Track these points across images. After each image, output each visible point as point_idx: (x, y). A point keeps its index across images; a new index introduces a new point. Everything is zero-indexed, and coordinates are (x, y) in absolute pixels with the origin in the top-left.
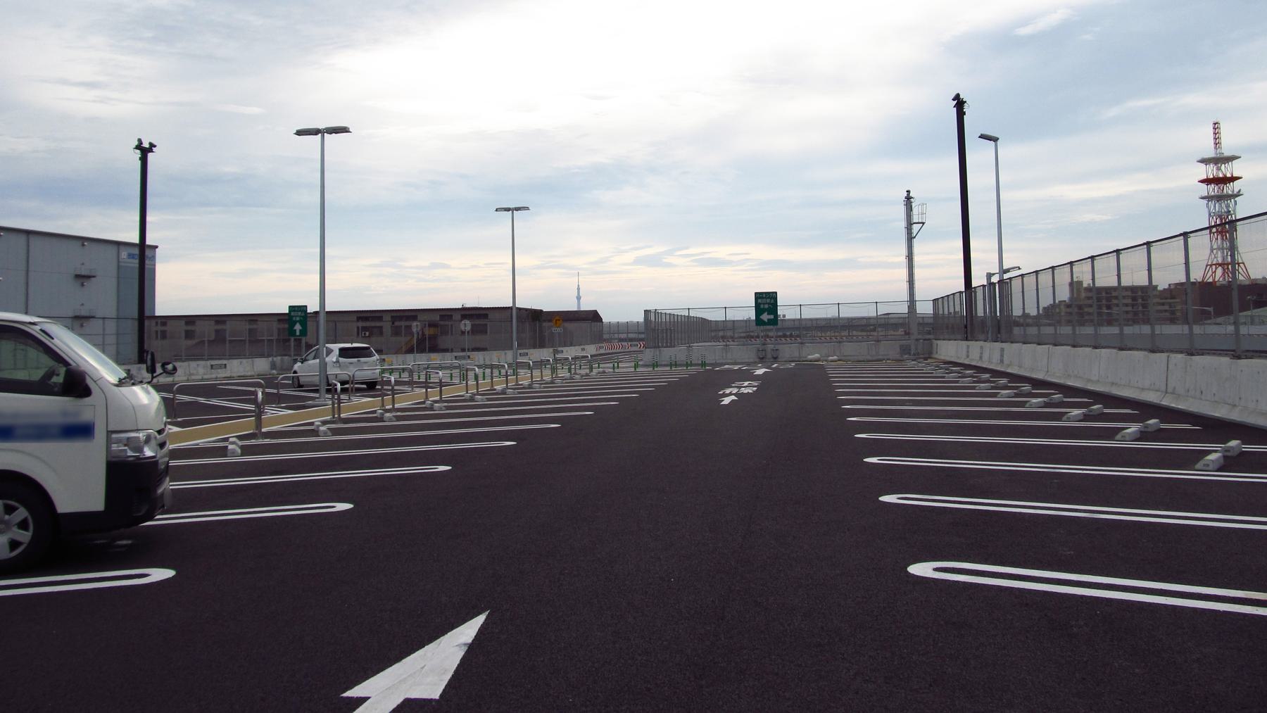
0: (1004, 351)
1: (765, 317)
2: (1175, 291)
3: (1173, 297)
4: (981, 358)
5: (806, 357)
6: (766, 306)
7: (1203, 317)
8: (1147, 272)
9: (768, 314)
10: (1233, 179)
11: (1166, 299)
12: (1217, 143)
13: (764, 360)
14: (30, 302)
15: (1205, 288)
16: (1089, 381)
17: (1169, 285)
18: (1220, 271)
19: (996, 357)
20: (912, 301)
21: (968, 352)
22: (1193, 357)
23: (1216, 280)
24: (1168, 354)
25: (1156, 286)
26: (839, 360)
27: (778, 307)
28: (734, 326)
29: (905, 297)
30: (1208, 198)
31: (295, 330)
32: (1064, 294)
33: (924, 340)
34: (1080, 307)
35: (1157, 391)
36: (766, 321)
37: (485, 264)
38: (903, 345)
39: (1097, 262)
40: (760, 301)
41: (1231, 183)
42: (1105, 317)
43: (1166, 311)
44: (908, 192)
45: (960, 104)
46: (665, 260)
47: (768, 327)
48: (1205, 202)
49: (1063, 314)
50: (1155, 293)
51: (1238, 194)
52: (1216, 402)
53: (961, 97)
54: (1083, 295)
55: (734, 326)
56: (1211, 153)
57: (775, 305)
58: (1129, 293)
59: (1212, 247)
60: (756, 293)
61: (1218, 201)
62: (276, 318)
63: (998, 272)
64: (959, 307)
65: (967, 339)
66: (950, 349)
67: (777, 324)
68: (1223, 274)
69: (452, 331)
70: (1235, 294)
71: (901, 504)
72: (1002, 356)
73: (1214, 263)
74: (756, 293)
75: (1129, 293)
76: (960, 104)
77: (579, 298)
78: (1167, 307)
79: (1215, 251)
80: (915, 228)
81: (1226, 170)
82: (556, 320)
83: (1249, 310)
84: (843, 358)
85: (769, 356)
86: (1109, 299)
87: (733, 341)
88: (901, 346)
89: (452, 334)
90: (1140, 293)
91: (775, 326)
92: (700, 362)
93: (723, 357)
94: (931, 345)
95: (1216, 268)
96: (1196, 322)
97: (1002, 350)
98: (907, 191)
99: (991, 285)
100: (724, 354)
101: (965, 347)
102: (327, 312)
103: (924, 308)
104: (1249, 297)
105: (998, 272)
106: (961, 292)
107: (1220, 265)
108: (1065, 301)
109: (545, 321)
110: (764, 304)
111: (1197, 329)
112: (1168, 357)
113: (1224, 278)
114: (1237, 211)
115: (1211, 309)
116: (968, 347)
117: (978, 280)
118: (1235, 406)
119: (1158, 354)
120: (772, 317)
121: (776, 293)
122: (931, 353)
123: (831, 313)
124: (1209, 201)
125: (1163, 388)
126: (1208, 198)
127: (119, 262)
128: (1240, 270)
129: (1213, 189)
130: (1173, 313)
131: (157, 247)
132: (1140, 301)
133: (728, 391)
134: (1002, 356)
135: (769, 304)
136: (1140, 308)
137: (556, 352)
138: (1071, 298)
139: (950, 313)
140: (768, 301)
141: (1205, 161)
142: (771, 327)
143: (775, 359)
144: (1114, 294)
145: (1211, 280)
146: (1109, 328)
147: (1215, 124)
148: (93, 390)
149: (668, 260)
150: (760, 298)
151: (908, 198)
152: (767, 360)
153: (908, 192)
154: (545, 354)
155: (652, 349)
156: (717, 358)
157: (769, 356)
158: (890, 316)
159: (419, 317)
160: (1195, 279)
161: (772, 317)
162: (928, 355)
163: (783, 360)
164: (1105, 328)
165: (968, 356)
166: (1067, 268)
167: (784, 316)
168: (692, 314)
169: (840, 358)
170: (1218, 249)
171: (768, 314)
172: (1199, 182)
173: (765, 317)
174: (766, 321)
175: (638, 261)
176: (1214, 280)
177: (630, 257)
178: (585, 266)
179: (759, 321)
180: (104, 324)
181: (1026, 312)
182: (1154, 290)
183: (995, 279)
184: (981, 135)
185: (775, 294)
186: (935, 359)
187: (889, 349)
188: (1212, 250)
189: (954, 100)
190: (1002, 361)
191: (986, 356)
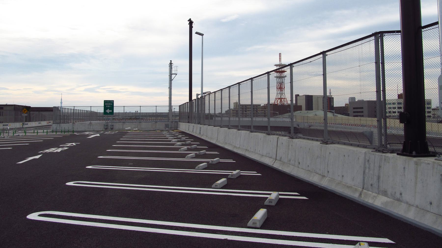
0: (201, 128)
1: (108, 111)
2: (265, 107)
3: (265, 109)
5: (125, 128)
6: (109, 106)
7: (274, 115)
9: (109, 110)
11: (263, 109)
12: (280, 60)
13: (107, 130)
15: (275, 106)
16: (235, 147)
17: (264, 105)
18: (279, 101)
19: (198, 131)
20: (170, 106)
21: (189, 128)
22: (294, 140)
23: (278, 103)
24: (278, 136)
26: (138, 130)
27: (114, 107)
28: (119, 115)
29: (167, 104)
31: (109, 112)
33: (175, 122)
35: (270, 158)
36: (109, 113)
37: (24, 89)
38: (166, 124)
40: (106, 104)
42: (244, 114)
44: (171, 61)
45: (191, 22)
46: (96, 90)
48: (276, 78)
50: (260, 107)
52: (309, 171)
53: (191, 20)
55: (119, 115)
56: (278, 63)
59: (277, 93)
60: (104, 101)
61: (280, 78)
62: (13, 107)
63: (201, 93)
65: (189, 122)
66: (184, 127)
68: (280, 102)
69: (3, 114)
70: (209, 116)
72: (200, 131)
74: (104, 101)
76: (191, 22)
77: (61, 103)
78: (263, 112)
80: (173, 76)
82: (24, 111)
83: (288, 113)
84: (140, 129)
85: (109, 128)
86: (246, 109)
87: (103, 121)
88: (165, 124)
89: (3, 115)
90: (255, 107)
91: (112, 115)
92: (61, 130)
93: (89, 128)
94: (178, 124)
95: (278, 100)
96: (271, 117)
97: (200, 128)
98: (171, 61)
99: (198, 98)
100: (89, 127)
101: (188, 126)
105: (201, 93)
106: (188, 103)
107: (279, 99)
108: (232, 109)
109: (31, 111)
110: (108, 105)
111: (272, 119)
112: (278, 138)
114: (285, 82)
115: (278, 113)
117: (194, 97)
118: (324, 176)
119: (272, 136)
120: (111, 111)
121: (113, 101)
122: (177, 127)
123: (153, 110)
125: (274, 156)
126: (277, 77)
130: (265, 113)
132: (255, 109)
134: (200, 131)
135: (110, 105)
137: (23, 124)
138: (234, 108)
140: (110, 104)
142: (111, 115)
143: (112, 129)
144: (247, 107)
145: (276, 103)
146: (246, 118)
147: (280, 54)
149: (98, 90)
150: (106, 103)
151: (171, 64)
152: (108, 130)
153: (171, 61)
154: (18, 125)
155: (56, 124)
156: (86, 128)
157: (109, 128)
158: (175, 112)
159: (4, 108)
160: (272, 103)
161: (111, 111)
162: (176, 128)
163: (115, 130)
164: (244, 118)
165: (189, 130)
166: (227, 90)
169: (139, 129)
170: (279, 93)
171: (109, 110)
173: (108, 111)
174: (109, 113)
175: (86, 90)
176: (277, 103)
177: (83, 88)
178: (65, 91)
179: (105, 113)
183: (199, 97)
184: (196, 32)
186: (178, 130)
187: (160, 125)
188: (277, 94)
189: (188, 21)
190: (200, 133)
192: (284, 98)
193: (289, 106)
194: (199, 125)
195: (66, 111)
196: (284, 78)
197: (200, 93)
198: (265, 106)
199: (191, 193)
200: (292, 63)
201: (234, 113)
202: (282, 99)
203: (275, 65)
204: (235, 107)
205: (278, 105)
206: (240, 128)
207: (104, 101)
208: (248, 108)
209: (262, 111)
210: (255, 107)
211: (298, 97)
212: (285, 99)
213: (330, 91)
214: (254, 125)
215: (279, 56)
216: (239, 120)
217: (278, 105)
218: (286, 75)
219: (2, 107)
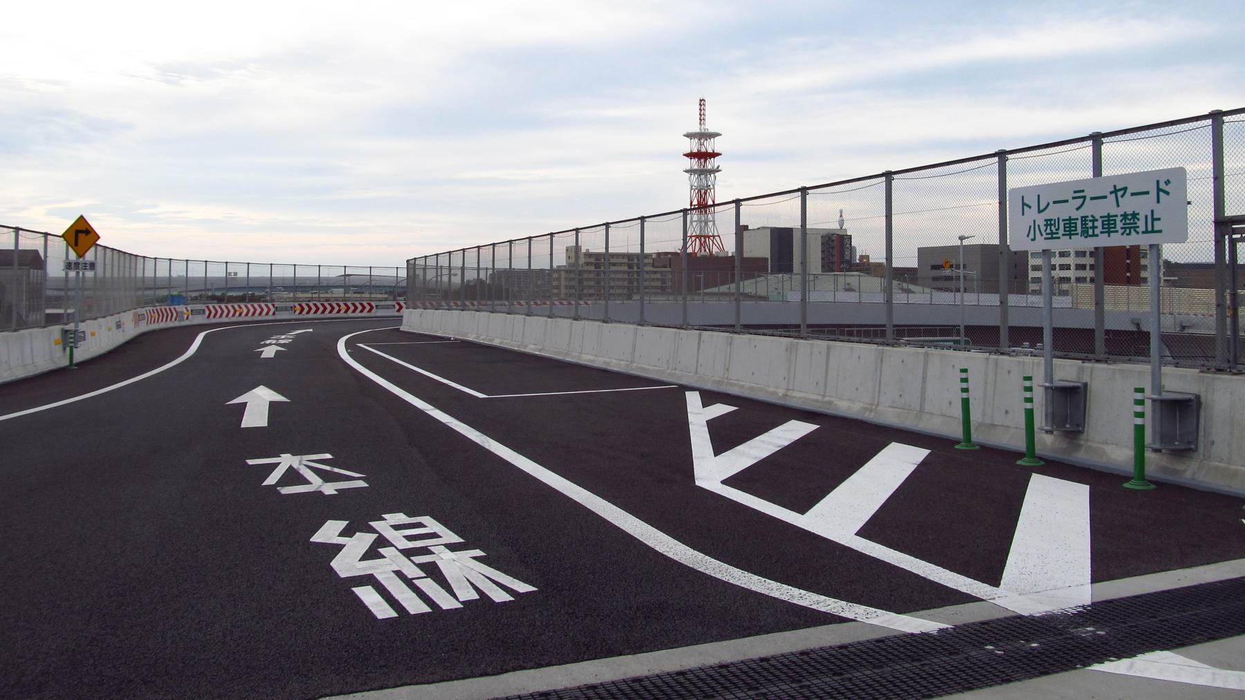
8: (48, 255)
10: (714, 155)
12: (702, 119)
30: (690, 171)
32: (561, 260)
34: (580, 273)
39: (581, 234)
41: (712, 159)
43: (658, 279)
48: (688, 175)
51: (718, 170)
54: (582, 260)
56: (696, 129)
58: (626, 260)
71: (103, 388)
73: (694, 234)
75: (626, 260)
78: (659, 276)
81: (709, 146)
90: (635, 261)
107: (697, 237)
124: (691, 175)
126: (690, 171)
129: (694, 164)
130: (664, 281)
132: (635, 269)
133: (268, 342)
136: (635, 276)
139: (119, 277)
141: (690, 136)
147: (701, 101)
148: (1000, 586)
167: (236, 274)
168: (324, 274)
172: (684, 155)
181: (480, 277)
192: (710, 234)
193: (728, 260)
195: (162, 272)
196: (712, 175)
199: (637, 648)
201: (571, 279)
202: (705, 237)
203: (685, 133)
204: (573, 261)
206: (804, 331)
208: (614, 264)
209: (655, 273)
210: (635, 261)
211: (745, 233)
212: (714, 237)
213: (841, 216)
214: (1011, 324)
215: (698, 107)
216: (1003, 302)
218: (718, 167)
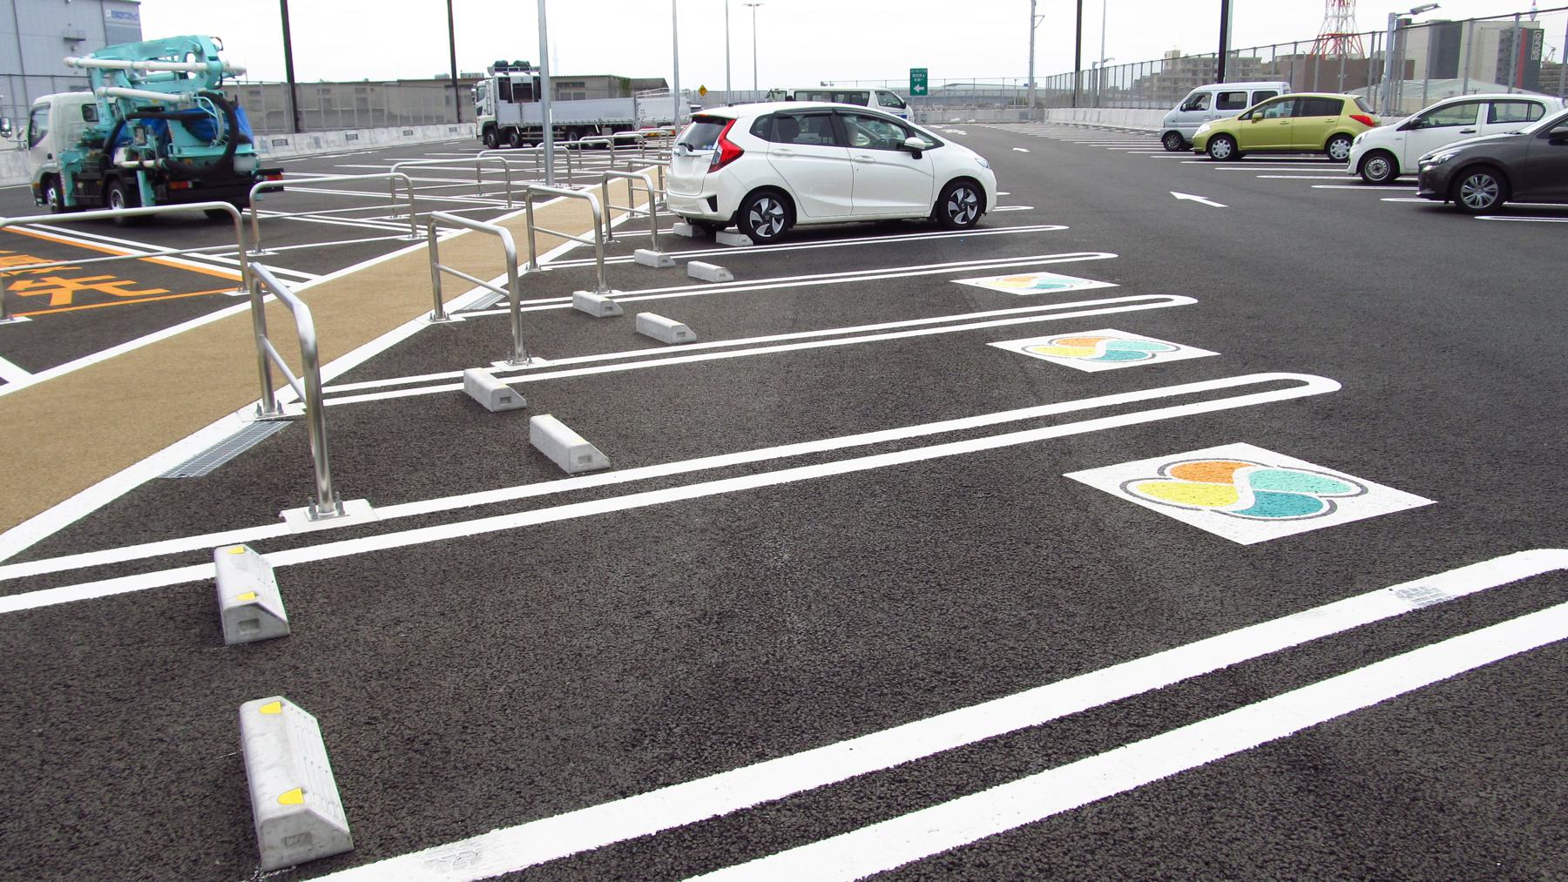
1: (918, 88)
4: (1084, 119)
6: (919, 80)
14: (25, 62)
16: (1144, 126)
25: (1260, 59)
34: (1176, 81)
40: (914, 75)
47: (920, 96)
49: (1155, 89)
50: (1257, 67)
54: (1179, 67)
57: (926, 79)
59: (1326, 14)
64: (1069, 85)
65: (1074, 107)
67: (926, 94)
72: (1099, 117)
79: (1329, 19)
94: (1043, 112)
97: (1099, 113)
101: (1073, 113)
102: (551, 78)
103: (1041, 84)
104: (492, 136)
113: (1336, 50)
116: (1075, 112)
120: (923, 88)
127: (104, 22)
128: (1354, 43)
131: (139, 3)
134: (1099, 117)
158: (957, 87)
161: (923, 88)
170: (1334, 16)
173: (918, 88)
179: (912, 92)
180: (53, 83)
182: (1256, 63)
183: (1098, 66)
185: (923, 73)
190: (1099, 120)
191: (1088, 118)
194: (1097, 109)
197: (1100, 60)
198: (1276, 64)
200: (1521, 12)
204: (1170, 68)
205: (1327, 58)
207: (911, 70)
217: (1327, 58)
219: (582, 81)
